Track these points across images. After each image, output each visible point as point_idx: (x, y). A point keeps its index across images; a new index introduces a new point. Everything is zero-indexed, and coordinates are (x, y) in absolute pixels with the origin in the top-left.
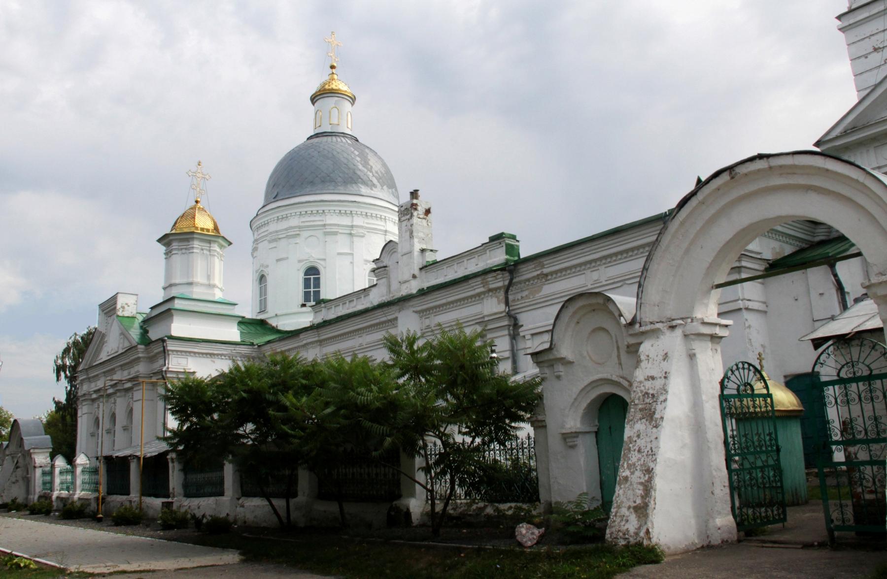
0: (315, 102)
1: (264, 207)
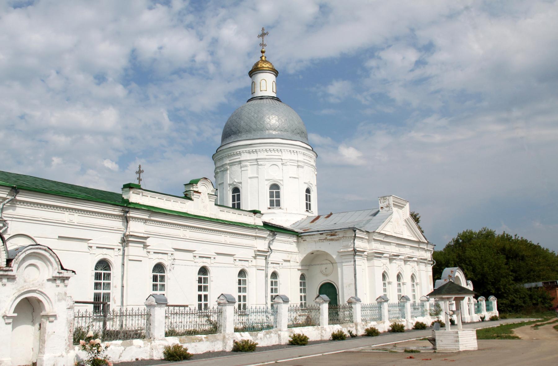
0: (252, 75)
1: (221, 147)
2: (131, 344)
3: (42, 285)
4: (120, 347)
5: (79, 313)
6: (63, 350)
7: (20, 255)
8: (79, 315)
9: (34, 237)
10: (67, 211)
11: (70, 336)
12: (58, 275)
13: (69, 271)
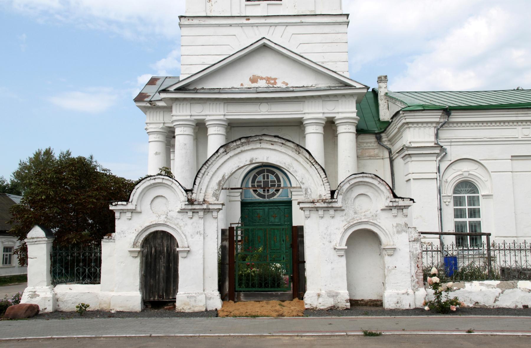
2: (514, 287)
3: (376, 216)
4: (494, 289)
5: (504, 245)
6: (409, 288)
7: (343, 186)
8: (505, 247)
9: (480, 160)
10: (520, 125)
11: (419, 271)
12: (391, 204)
13: (405, 199)
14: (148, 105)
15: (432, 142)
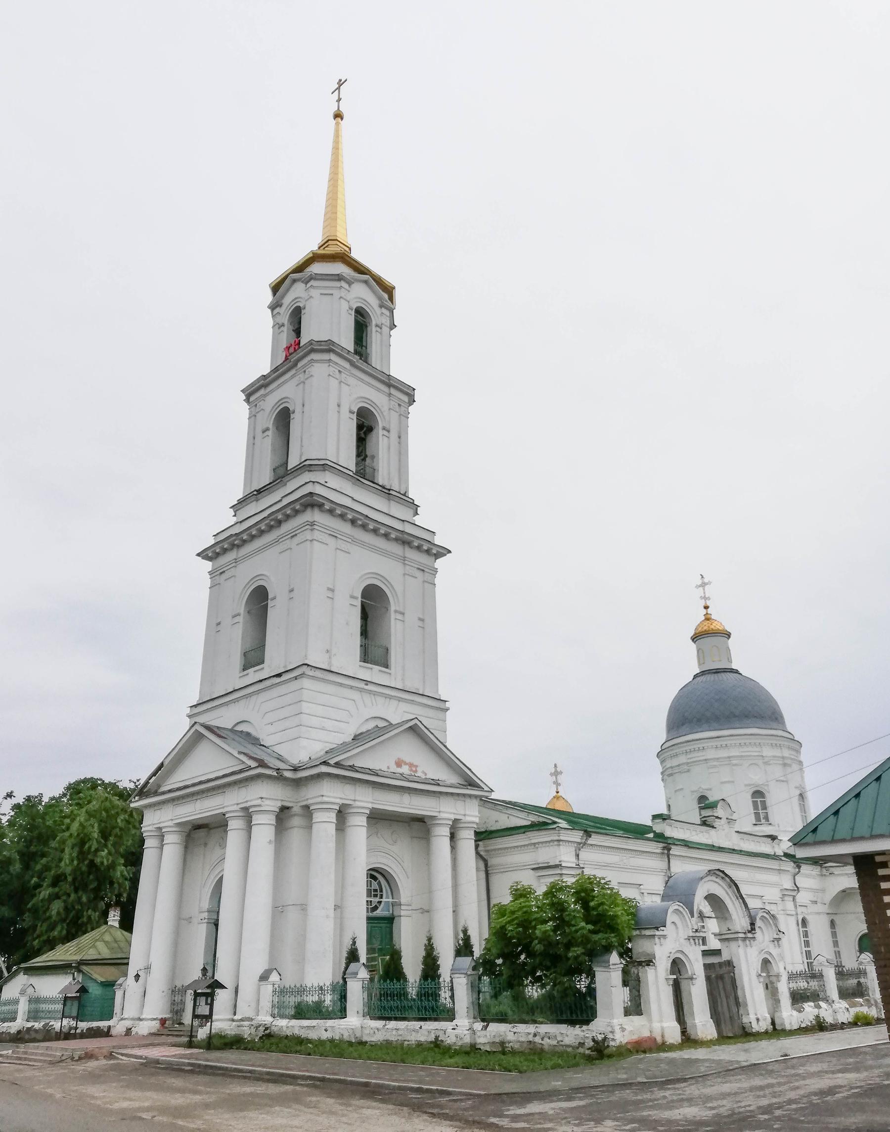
14: (275, 774)
15: (573, 862)
